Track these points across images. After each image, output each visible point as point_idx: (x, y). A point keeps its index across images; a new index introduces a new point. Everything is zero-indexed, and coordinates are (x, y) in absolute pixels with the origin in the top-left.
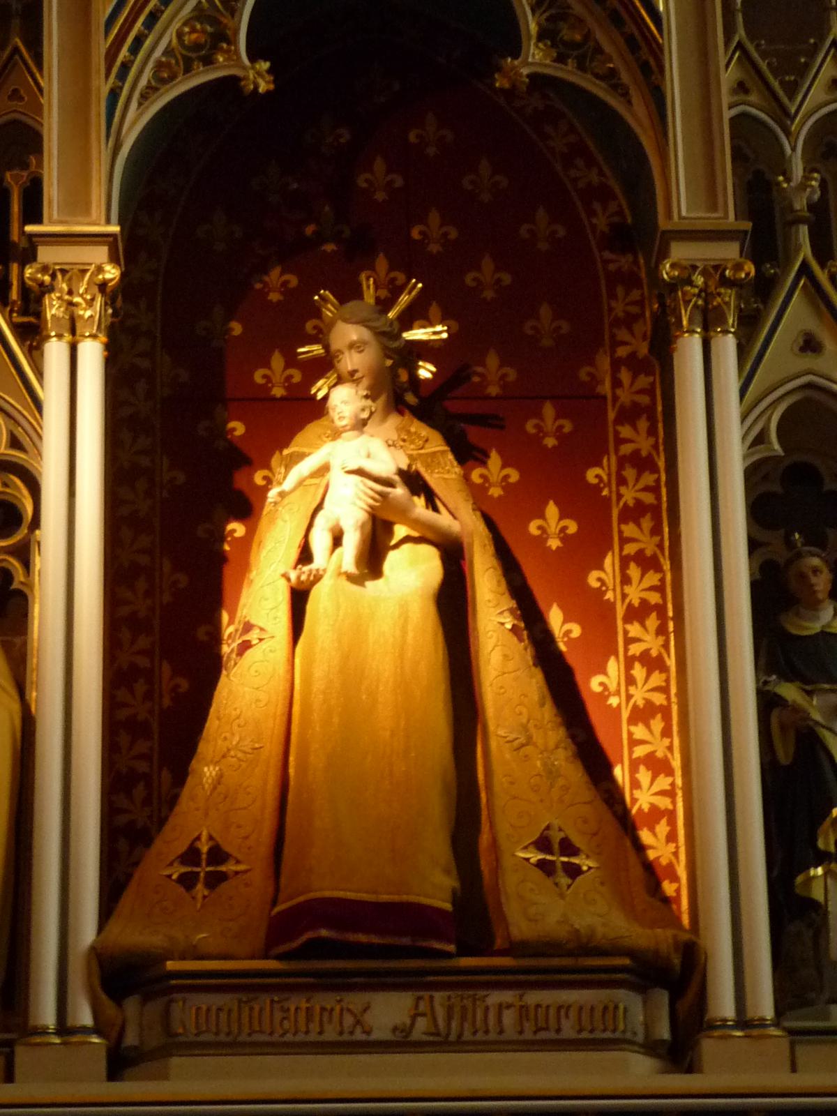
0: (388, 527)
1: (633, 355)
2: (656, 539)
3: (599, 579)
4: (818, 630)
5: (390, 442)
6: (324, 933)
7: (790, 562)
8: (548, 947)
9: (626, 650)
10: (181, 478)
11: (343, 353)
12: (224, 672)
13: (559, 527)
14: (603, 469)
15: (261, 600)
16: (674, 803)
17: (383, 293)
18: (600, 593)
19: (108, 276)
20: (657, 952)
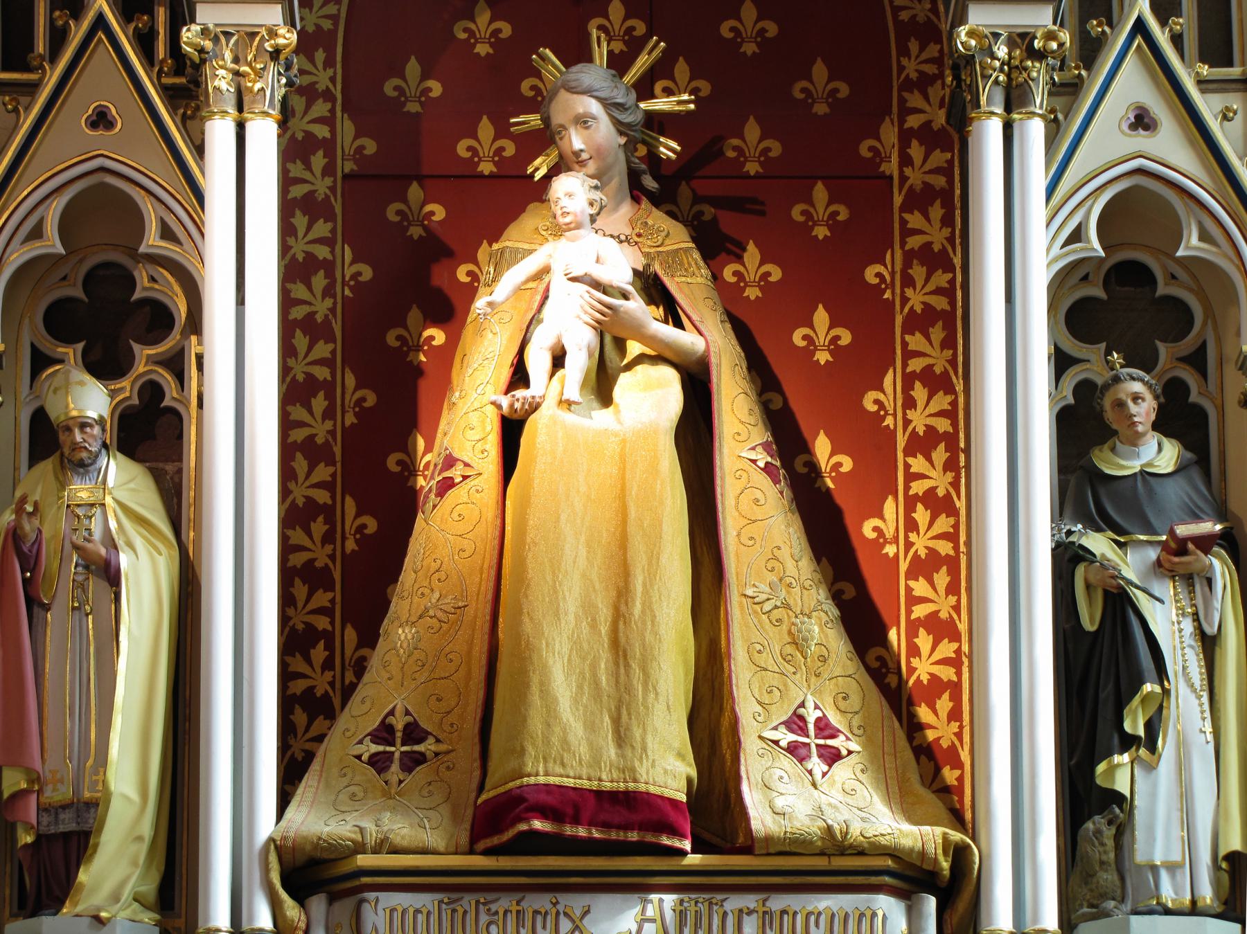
0: (620, 344)
1: (927, 125)
2: (948, 353)
3: (877, 402)
4: (1137, 470)
5: (623, 237)
6: (538, 824)
7: (1106, 387)
8: (793, 846)
9: (907, 488)
10: (367, 273)
11: (565, 129)
12: (420, 515)
13: (829, 337)
14: (886, 267)
15: (465, 427)
16: (959, 674)
17: (618, 46)
18: (878, 418)
19: (281, 41)
20: (923, 854)
